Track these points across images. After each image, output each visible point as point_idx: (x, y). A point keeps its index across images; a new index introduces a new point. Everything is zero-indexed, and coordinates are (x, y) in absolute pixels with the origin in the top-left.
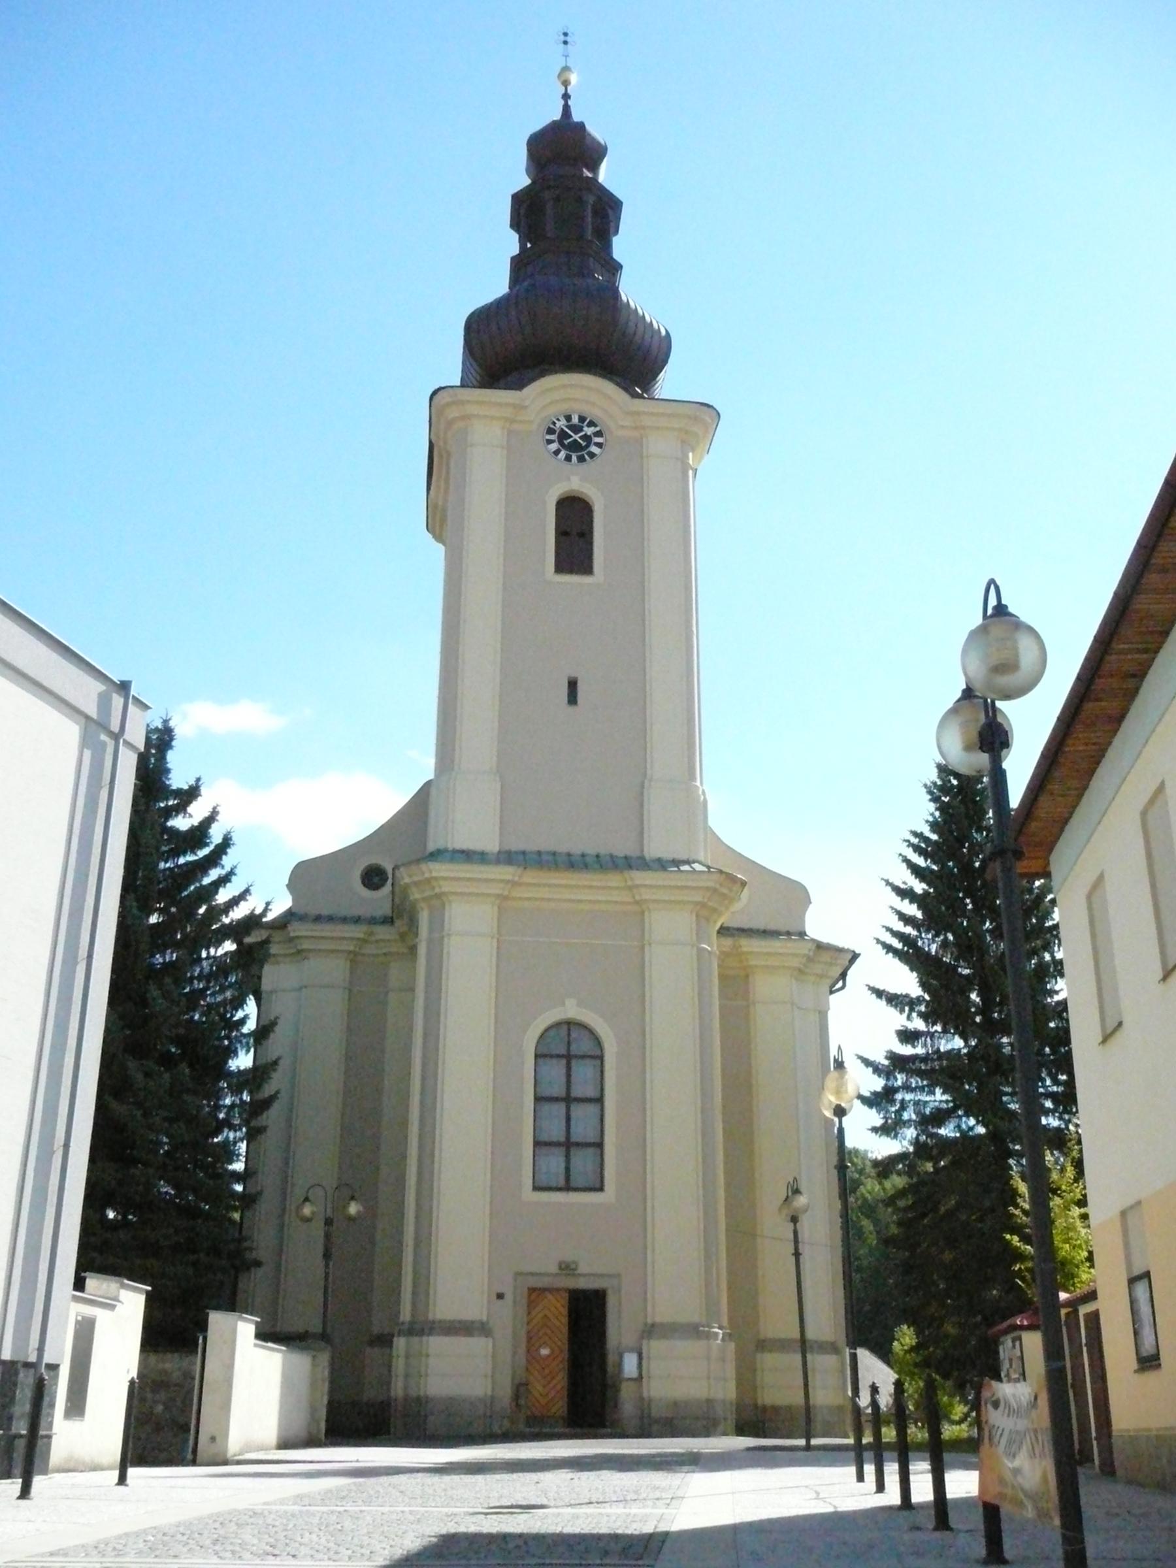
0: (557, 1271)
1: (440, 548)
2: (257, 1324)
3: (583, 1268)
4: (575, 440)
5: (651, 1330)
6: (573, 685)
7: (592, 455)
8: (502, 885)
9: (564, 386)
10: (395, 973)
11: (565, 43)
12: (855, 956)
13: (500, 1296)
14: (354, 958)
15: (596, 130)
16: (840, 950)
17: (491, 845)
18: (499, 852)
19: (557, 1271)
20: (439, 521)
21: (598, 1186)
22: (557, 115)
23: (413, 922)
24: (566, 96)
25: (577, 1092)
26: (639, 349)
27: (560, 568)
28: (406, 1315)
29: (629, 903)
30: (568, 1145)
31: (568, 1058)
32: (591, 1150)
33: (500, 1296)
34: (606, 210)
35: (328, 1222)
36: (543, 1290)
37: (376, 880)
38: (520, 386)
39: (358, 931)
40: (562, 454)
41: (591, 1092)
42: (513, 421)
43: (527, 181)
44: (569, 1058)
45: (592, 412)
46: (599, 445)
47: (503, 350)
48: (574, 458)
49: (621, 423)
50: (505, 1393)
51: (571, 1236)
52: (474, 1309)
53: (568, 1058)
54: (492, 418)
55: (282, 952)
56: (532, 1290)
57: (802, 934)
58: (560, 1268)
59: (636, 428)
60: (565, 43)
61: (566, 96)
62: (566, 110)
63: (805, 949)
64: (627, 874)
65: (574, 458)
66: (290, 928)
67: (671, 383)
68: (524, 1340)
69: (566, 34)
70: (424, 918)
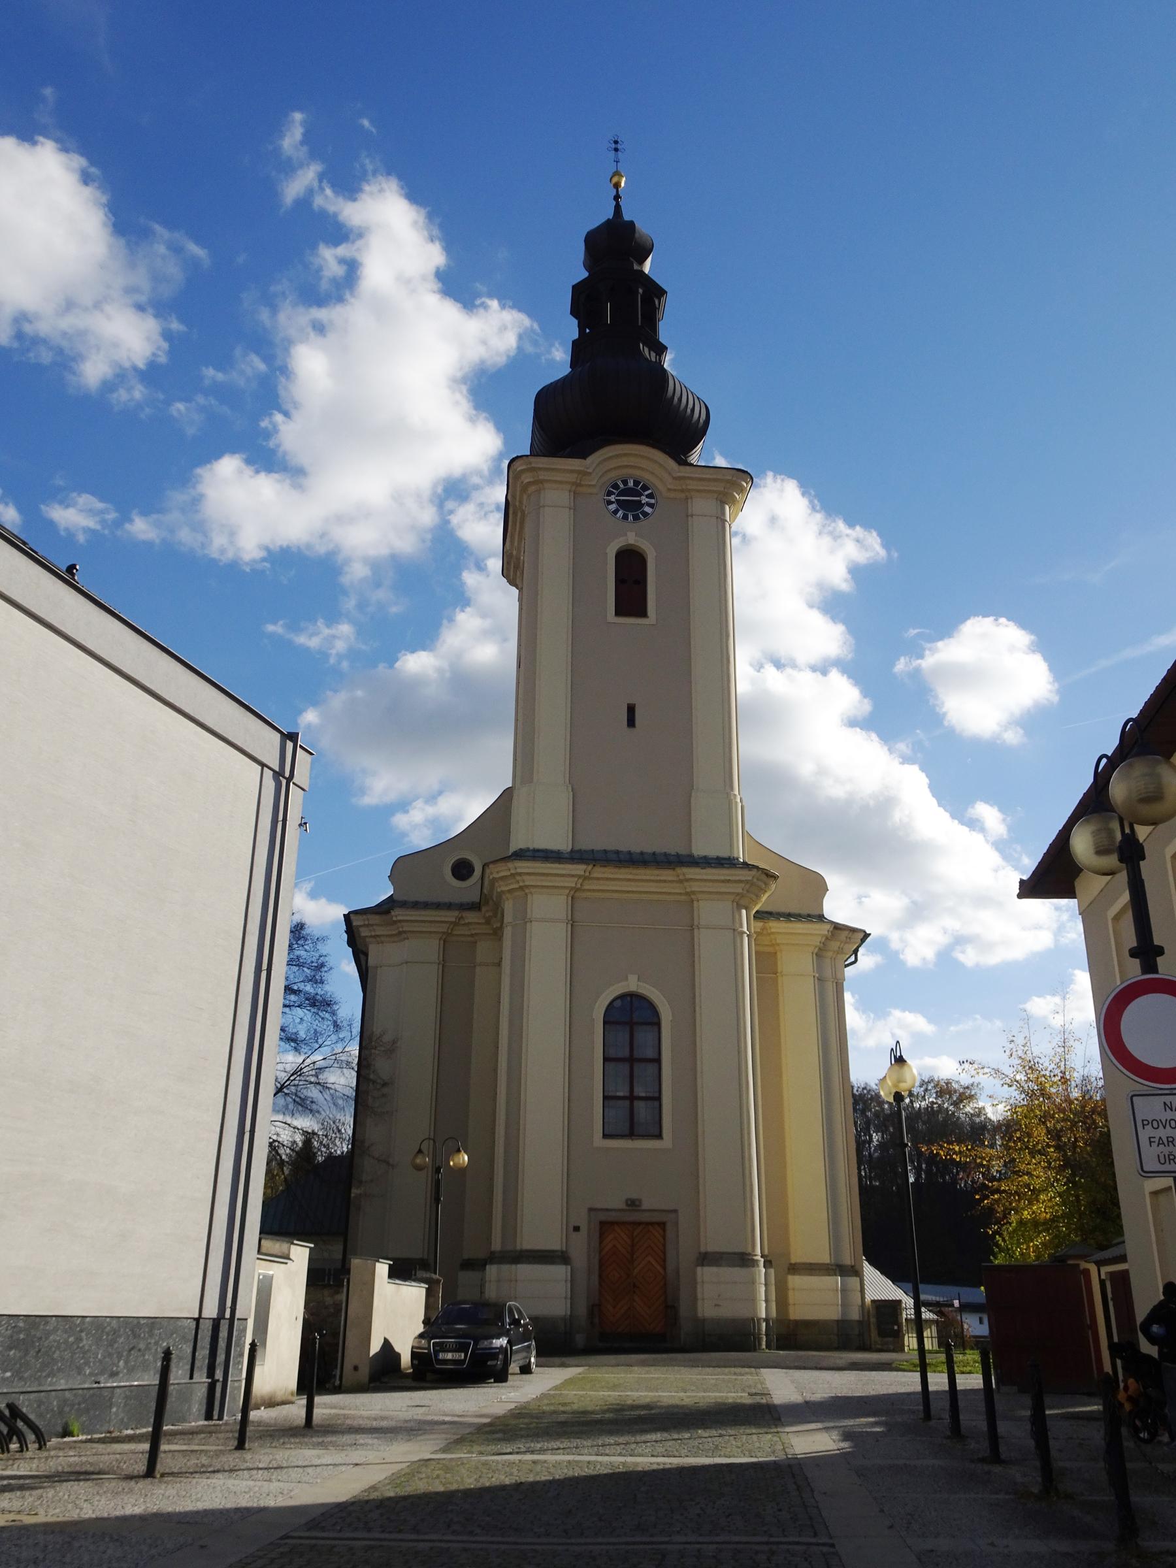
0: (624, 1207)
3: (645, 1206)
4: (630, 500)
5: (707, 1259)
7: (645, 514)
9: (618, 456)
10: (483, 950)
11: (616, 150)
13: (577, 1229)
14: (446, 940)
15: (644, 227)
16: (854, 930)
17: (562, 844)
18: (572, 851)
19: (624, 1207)
22: (609, 214)
23: (498, 911)
24: (617, 197)
26: (1065, 1081)
29: (680, 894)
31: (632, 1098)
33: (577, 1229)
36: (612, 1223)
38: (584, 456)
39: (451, 916)
42: (579, 485)
43: (586, 274)
44: (631, 1025)
45: (646, 477)
48: (630, 518)
49: (671, 487)
50: (582, 1310)
51: (632, 1173)
54: (561, 482)
55: (385, 933)
56: (602, 1223)
57: (821, 918)
58: (627, 1205)
59: (682, 491)
60: (616, 150)
61: (617, 197)
62: (618, 208)
63: (825, 929)
64: (679, 870)
65: (630, 518)
66: (393, 913)
67: (710, 454)
68: (597, 1267)
70: (508, 906)
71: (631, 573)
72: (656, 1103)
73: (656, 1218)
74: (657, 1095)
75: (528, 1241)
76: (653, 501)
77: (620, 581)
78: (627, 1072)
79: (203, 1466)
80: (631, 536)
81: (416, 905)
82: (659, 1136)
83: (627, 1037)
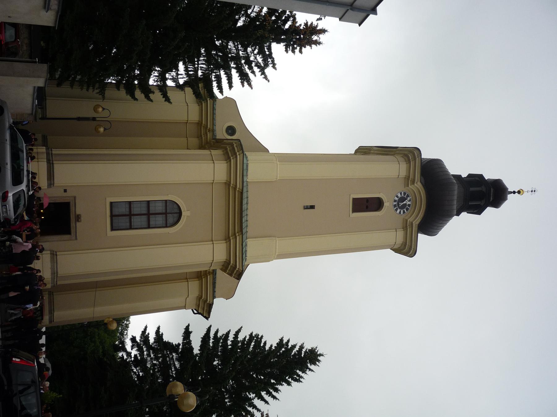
1: (353, 152)
2: (54, 27)
3: (78, 224)
6: (312, 207)
7: (396, 210)
8: (241, 188)
9: (421, 196)
11: (532, 191)
12: (207, 318)
13: (65, 191)
20: (363, 151)
21: (114, 228)
25: (152, 218)
27: (354, 199)
28: (55, 151)
30: (130, 215)
31: (166, 213)
32: (128, 224)
33: (65, 191)
34: (478, 210)
35: (94, 119)
37: (230, 132)
40: (396, 199)
41: (152, 223)
46: (400, 213)
47: (432, 173)
51: (92, 216)
52: (59, 180)
53: (166, 213)
57: (214, 297)
60: (532, 191)
62: (511, 193)
69: (535, 191)
71: (375, 204)
72: (164, 225)
73: (73, 231)
74: (133, 227)
75: (58, 168)
76: (402, 213)
77: (367, 200)
78: (143, 212)
79: (249, 63)
80: (388, 204)
81: (214, 109)
82: (112, 229)
83: (160, 212)
